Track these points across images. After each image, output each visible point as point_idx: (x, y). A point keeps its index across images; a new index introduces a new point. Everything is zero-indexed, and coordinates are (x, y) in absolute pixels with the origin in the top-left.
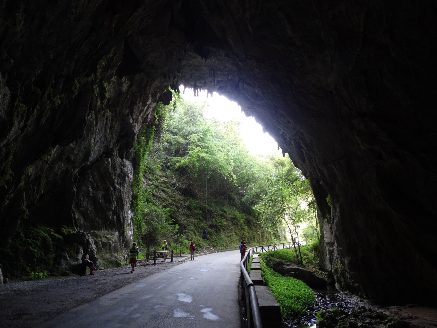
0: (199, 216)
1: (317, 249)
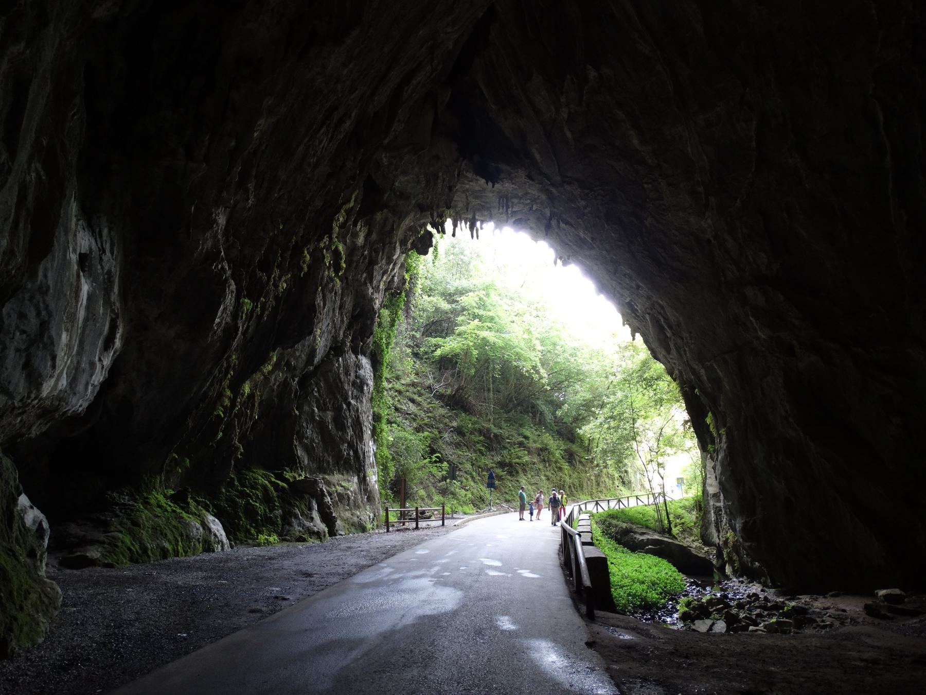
0: (479, 446)
1: (700, 506)
